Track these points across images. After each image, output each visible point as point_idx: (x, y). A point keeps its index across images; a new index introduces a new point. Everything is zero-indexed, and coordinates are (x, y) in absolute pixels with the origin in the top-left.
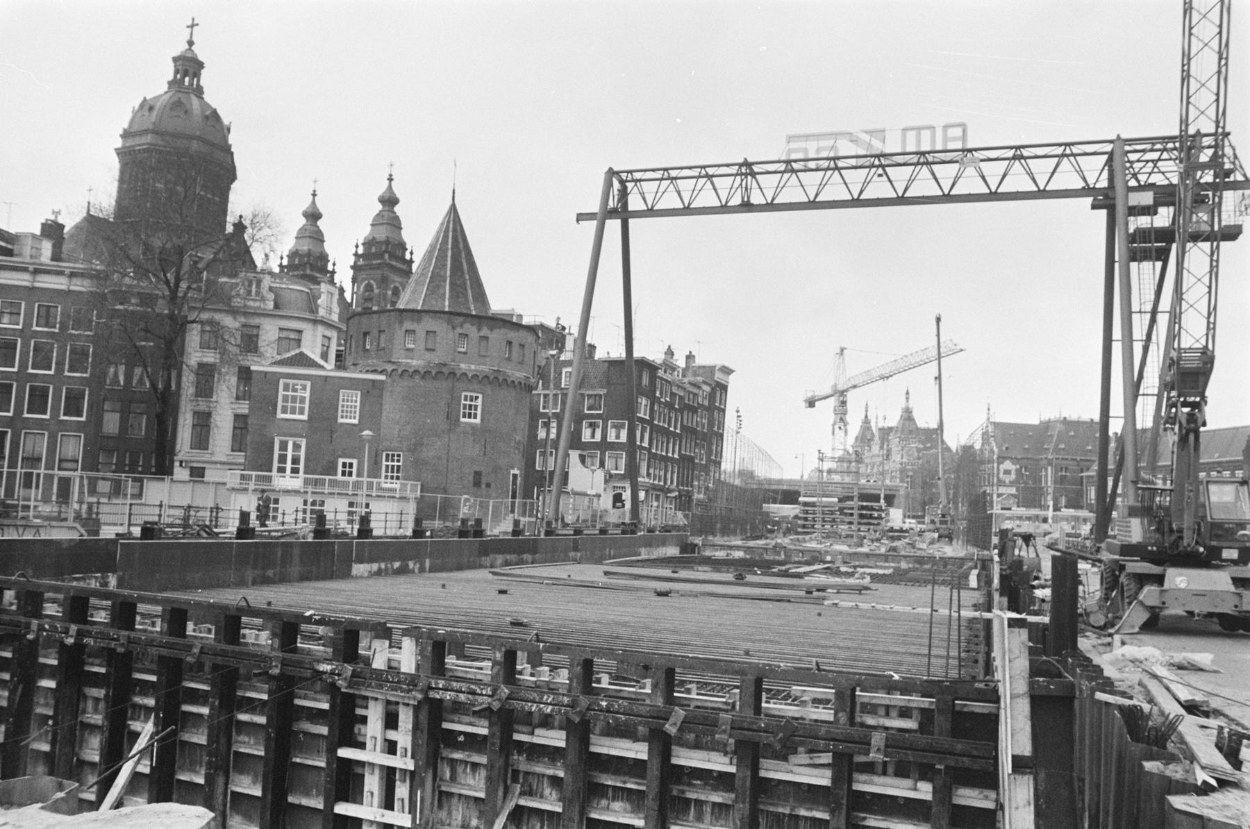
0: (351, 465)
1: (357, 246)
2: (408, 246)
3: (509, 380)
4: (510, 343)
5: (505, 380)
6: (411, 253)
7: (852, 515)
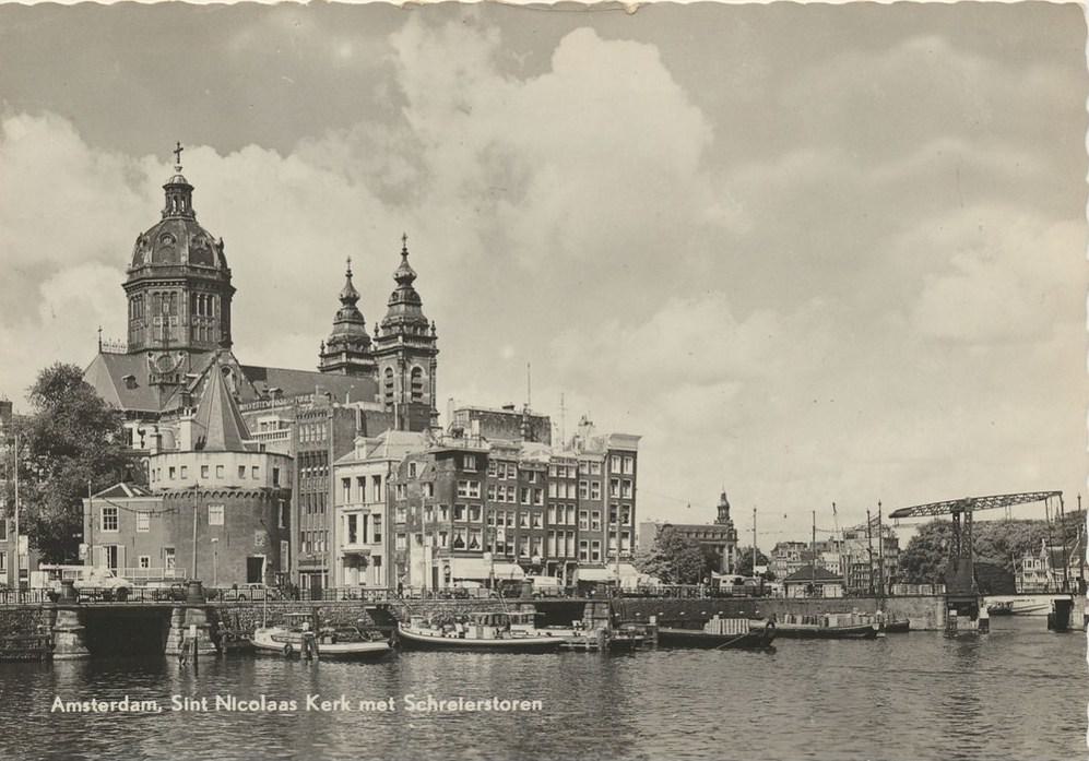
0: (147, 559)
1: (323, 348)
2: (430, 323)
6: (433, 329)
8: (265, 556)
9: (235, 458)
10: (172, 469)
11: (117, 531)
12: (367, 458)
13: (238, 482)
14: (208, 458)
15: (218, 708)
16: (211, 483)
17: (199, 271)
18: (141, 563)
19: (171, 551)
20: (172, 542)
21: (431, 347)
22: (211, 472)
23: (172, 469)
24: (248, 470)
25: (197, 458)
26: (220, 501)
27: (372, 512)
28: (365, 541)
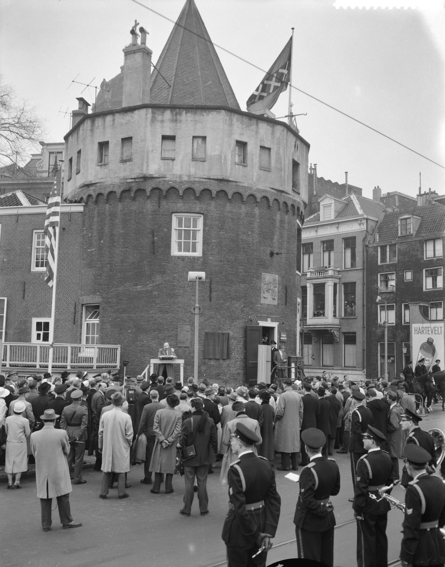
3: (259, 196)
4: (242, 145)
5: (238, 194)
13: (232, 171)
24: (253, 149)
25: (153, 120)
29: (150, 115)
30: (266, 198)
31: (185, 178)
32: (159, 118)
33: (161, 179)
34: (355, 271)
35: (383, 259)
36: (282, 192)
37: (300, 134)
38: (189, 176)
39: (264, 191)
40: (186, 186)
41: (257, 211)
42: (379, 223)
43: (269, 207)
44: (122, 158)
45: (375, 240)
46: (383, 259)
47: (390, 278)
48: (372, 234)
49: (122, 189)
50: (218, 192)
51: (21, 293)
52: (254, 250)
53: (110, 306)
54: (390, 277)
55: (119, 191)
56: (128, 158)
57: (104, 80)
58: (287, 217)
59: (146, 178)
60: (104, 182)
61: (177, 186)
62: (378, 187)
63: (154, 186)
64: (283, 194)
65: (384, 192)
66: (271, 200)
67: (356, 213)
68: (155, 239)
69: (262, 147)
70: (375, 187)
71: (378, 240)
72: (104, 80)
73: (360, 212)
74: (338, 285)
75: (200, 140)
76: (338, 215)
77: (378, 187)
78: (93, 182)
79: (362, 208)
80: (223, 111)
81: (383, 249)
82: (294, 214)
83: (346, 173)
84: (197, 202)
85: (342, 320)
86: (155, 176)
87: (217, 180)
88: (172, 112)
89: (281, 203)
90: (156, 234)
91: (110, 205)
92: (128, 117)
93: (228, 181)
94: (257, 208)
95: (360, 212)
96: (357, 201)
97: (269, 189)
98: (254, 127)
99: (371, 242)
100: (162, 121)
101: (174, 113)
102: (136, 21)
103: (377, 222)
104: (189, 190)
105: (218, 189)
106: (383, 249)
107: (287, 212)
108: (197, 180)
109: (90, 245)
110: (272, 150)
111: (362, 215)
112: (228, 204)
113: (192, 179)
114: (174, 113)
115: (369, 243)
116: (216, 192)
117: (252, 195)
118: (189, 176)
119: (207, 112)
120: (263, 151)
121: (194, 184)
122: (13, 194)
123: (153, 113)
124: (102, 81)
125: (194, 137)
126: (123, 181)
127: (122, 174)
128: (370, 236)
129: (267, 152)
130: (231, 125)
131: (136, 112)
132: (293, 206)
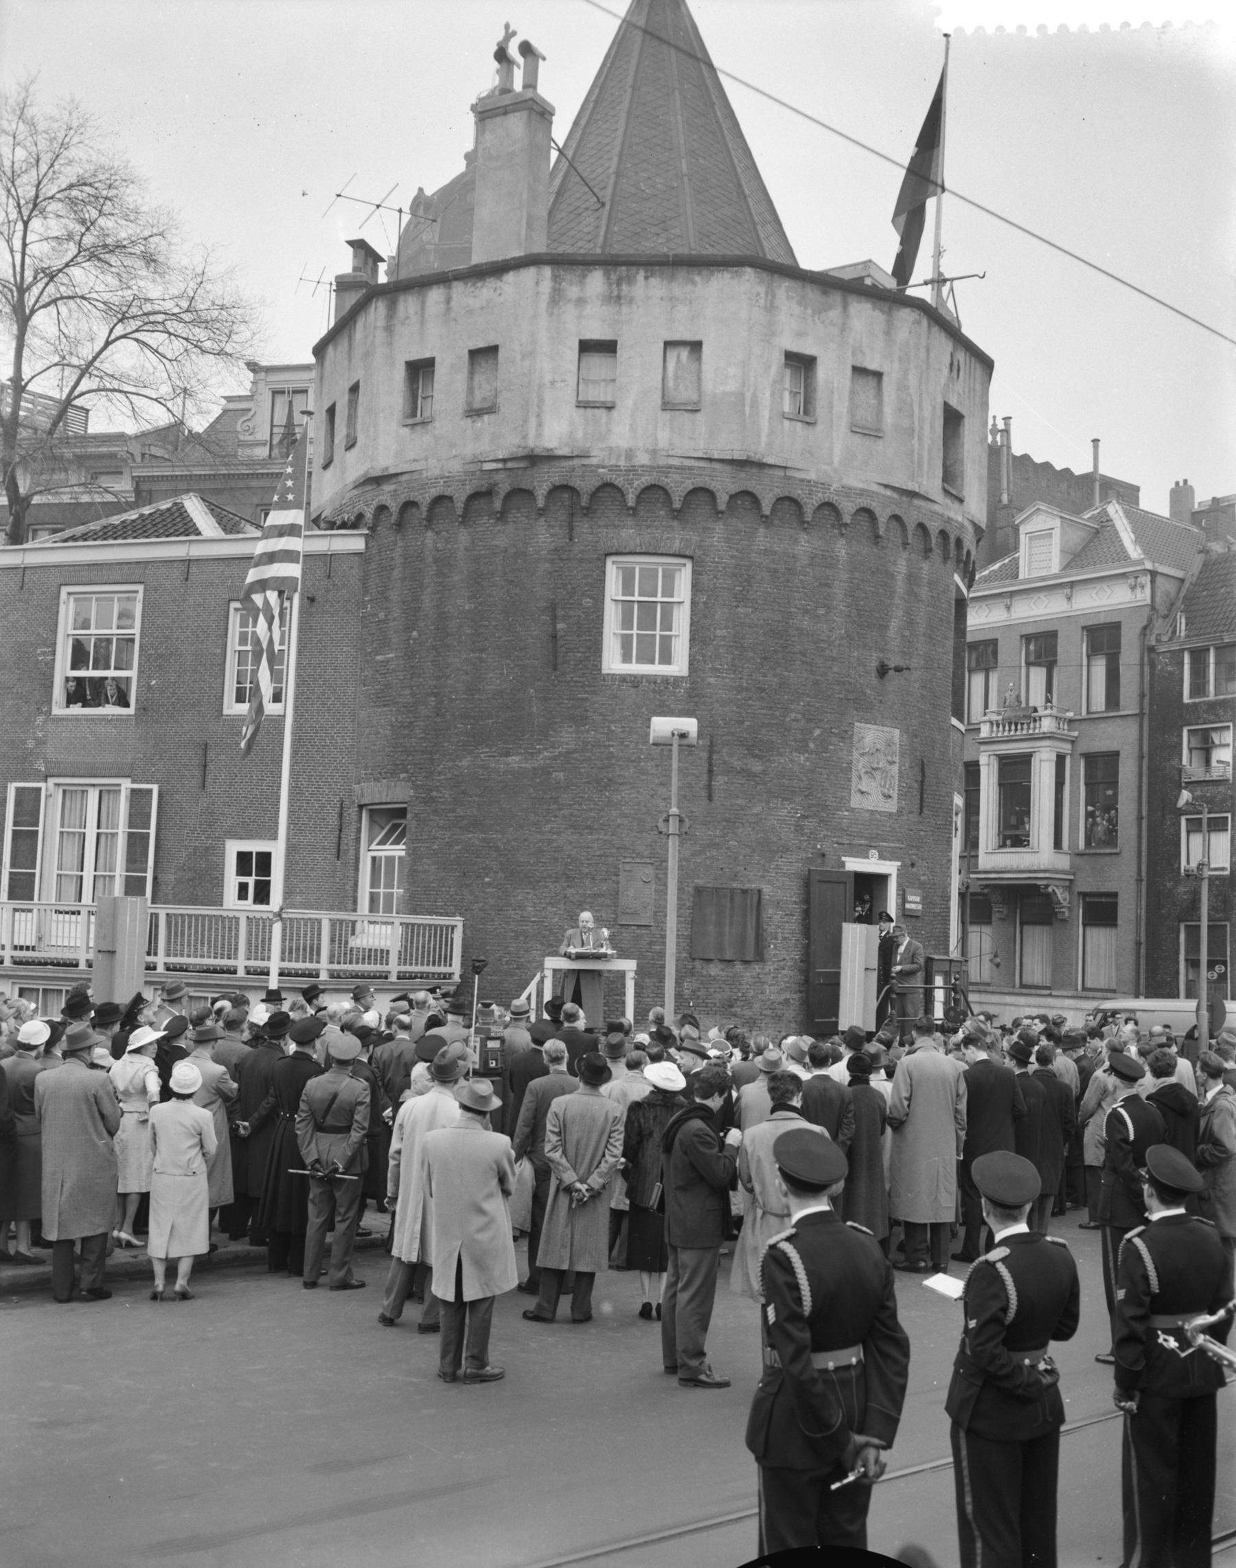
3: (847, 508)
4: (801, 364)
7: (444, 562)
8: (890, 868)
9: (771, 294)
10: (420, 370)
11: (131, 711)
12: (1066, 567)
13: (771, 435)
14: (615, 299)
15: (194, 507)
16: (633, 432)
17: (329, 1238)
18: (232, 880)
19: (391, 819)
20: (393, 771)
21: (228, 1076)
22: (639, 372)
23: (420, 370)
24: (831, 374)
25: (556, 297)
26: (678, 537)
27: (1084, 747)
28: (1058, 844)
29: (546, 286)
30: (867, 512)
31: (643, 459)
32: (573, 291)
33: (576, 462)
34: (1119, 721)
35: (1199, 687)
36: (913, 495)
37: (966, 330)
38: (654, 453)
39: (863, 493)
40: (646, 480)
41: (841, 549)
42: (1187, 585)
43: (877, 537)
44: (469, 404)
45: (1174, 632)
46: (1199, 687)
47: (1217, 742)
48: (1166, 617)
49: (469, 490)
50: (733, 497)
51: (197, 772)
52: (833, 659)
53: (435, 812)
54: (1216, 737)
55: (460, 499)
56: (486, 405)
57: (421, 190)
58: (925, 566)
59: (534, 459)
60: (420, 472)
61: (619, 482)
62: (1185, 481)
63: (557, 480)
64: (916, 502)
65: (1202, 496)
66: (882, 518)
67: (1123, 556)
68: (560, 626)
69: (858, 371)
70: (1177, 483)
71: (1183, 634)
72: (421, 190)
73: (1134, 552)
74: (1068, 760)
75: (684, 353)
76: (1073, 560)
77: (1185, 481)
78: (392, 471)
79: (1137, 541)
80: (749, 270)
81: (1199, 657)
82: (946, 558)
83: (1096, 441)
84: (675, 523)
85: (1078, 858)
86: (560, 453)
87: (732, 462)
88: (607, 275)
89: (911, 527)
90: (560, 613)
91: (437, 533)
92: (486, 290)
93: (762, 465)
94: (843, 541)
95: (1134, 552)
96: (1125, 521)
97: (875, 488)
98: (835, 314)
99: (1165, 638)
100: (581, 302)
101: (614, 277)
102: (507, 26)
103: (1182, 581)
104: (654, 492)
105: (734, 489)
106: (1199, 657)
107: (927, 551)
108: (675, 462)
109: (384, 645)
110: (885, 378)
111: (1141, 562)
112: (762, 530)
113: (662, 461)
114: (614, 277)
115: (1158, 641)
116: (725, 498)
117: (829, 506)
118: (654, 453)
119: (705, 272)
120: (862, 381)
121: (666, 474)
122: (175, 504)
123: (555, 278)
124: (415, 193)
125: (668, 344)
126: (472, 468)
127: (470, 449)
128: (1161, 620)
129: (872, 382)
130: (771, 308)
131: (510, 277)
132: (943, 534)
